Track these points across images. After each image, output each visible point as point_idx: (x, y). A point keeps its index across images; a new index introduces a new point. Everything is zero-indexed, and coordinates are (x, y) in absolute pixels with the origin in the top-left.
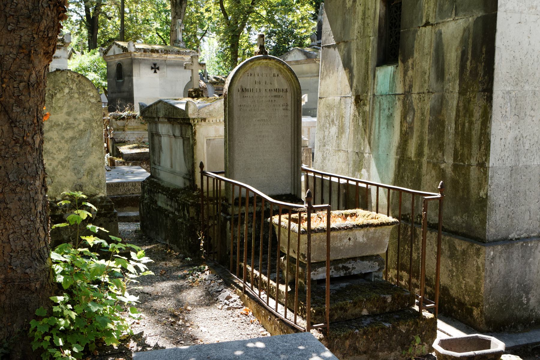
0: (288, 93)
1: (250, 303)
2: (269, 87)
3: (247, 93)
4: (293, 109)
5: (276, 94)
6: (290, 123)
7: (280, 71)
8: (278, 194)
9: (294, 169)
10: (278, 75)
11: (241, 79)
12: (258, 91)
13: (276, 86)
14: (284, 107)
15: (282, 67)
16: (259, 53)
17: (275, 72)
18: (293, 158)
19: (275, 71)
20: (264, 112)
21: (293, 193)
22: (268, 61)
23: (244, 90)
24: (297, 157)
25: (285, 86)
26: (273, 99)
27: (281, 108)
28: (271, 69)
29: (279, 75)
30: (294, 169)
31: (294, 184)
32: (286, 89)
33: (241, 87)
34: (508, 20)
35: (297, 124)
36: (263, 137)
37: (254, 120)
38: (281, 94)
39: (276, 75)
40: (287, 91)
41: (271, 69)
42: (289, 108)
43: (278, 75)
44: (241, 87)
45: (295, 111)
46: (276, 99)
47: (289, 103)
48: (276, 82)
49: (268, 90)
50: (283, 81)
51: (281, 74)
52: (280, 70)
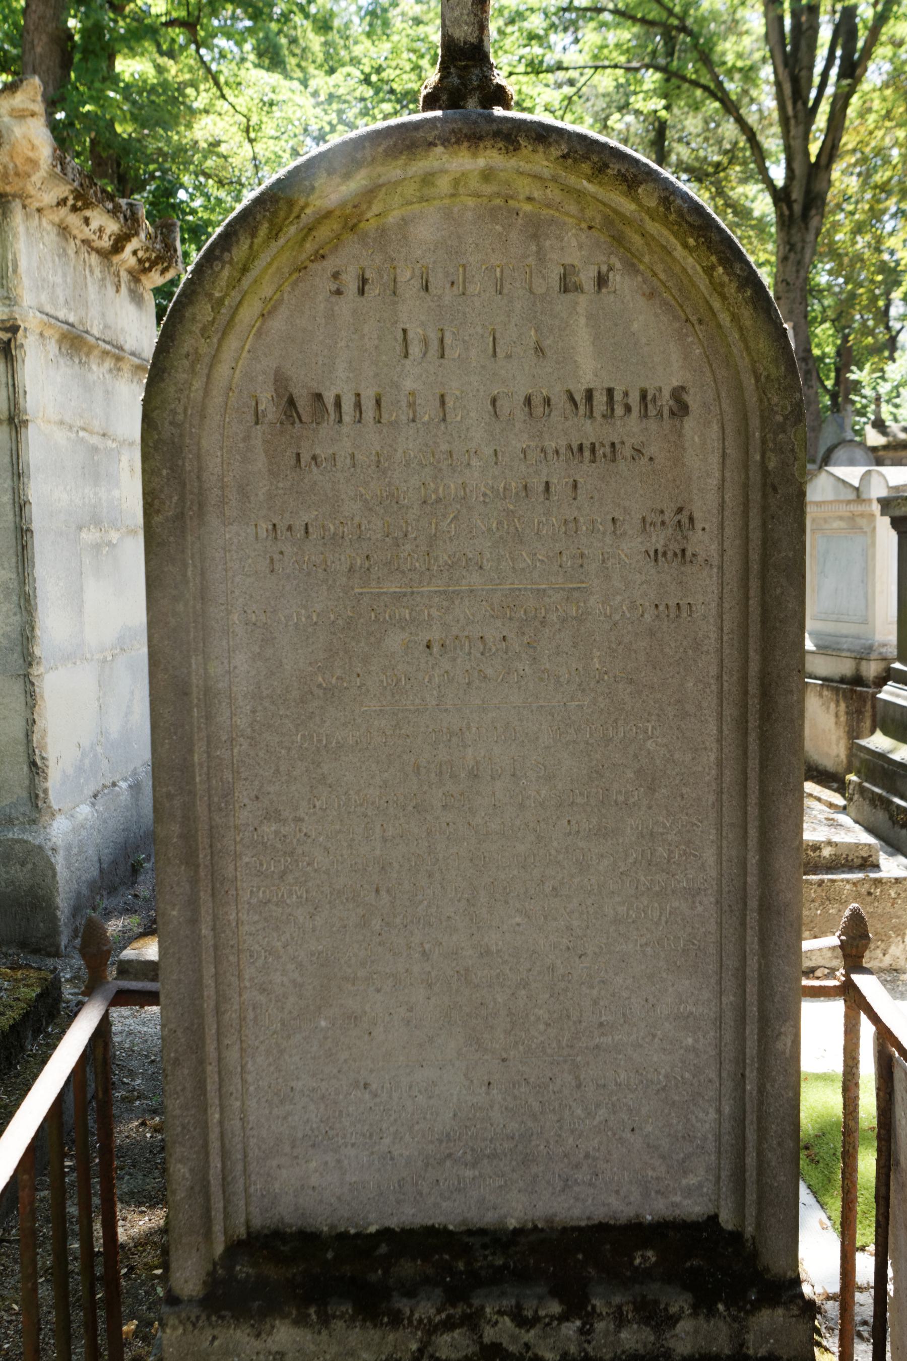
0: (689, 424)
1: (845, 144)
2: (520, 379)
3: (326, 429)
4: (733, 553)
5: (590, 431)
6: (708, 664)
7: (618, 240)
8: (600, 1214)
9: (741, 1038)
10: (601, 281)
11: (277, 324)
12: (428, 411)
13: (588, 371)
14: (658, 539)
15: (627, 206)
16: (431, 102)
17: (574, 257)
18: (731, 963)
19: (574, 249)
20: (475, 579)
21: (727, 1220)
22: (490, 157)
23: (303, 404)
24: (764, 939)
25: (668, 364)
26: (558, 473)
27: (633, 546)
28: (536, 230)
29: (616, 279)
30: (741, 1038)
31: (740, 1060)
32: (678, 394)
33: (280, 381)
34: (651, 459)
35: (765, 979)
36: (474, 775)
37: (395, 641)
38: (630, 429)
39: (587, 277)
40: (681, 409)
41: (536, 230)
42: (703, 542)
43: (601, 281)
44: (280, 381)
45: (744, 626)
46: (586, 473)
47: (704, 504)
48: (582, 340)
49: (512, 406)
50: (644, 320)
51: (631, 268)
52: (614, 231)
